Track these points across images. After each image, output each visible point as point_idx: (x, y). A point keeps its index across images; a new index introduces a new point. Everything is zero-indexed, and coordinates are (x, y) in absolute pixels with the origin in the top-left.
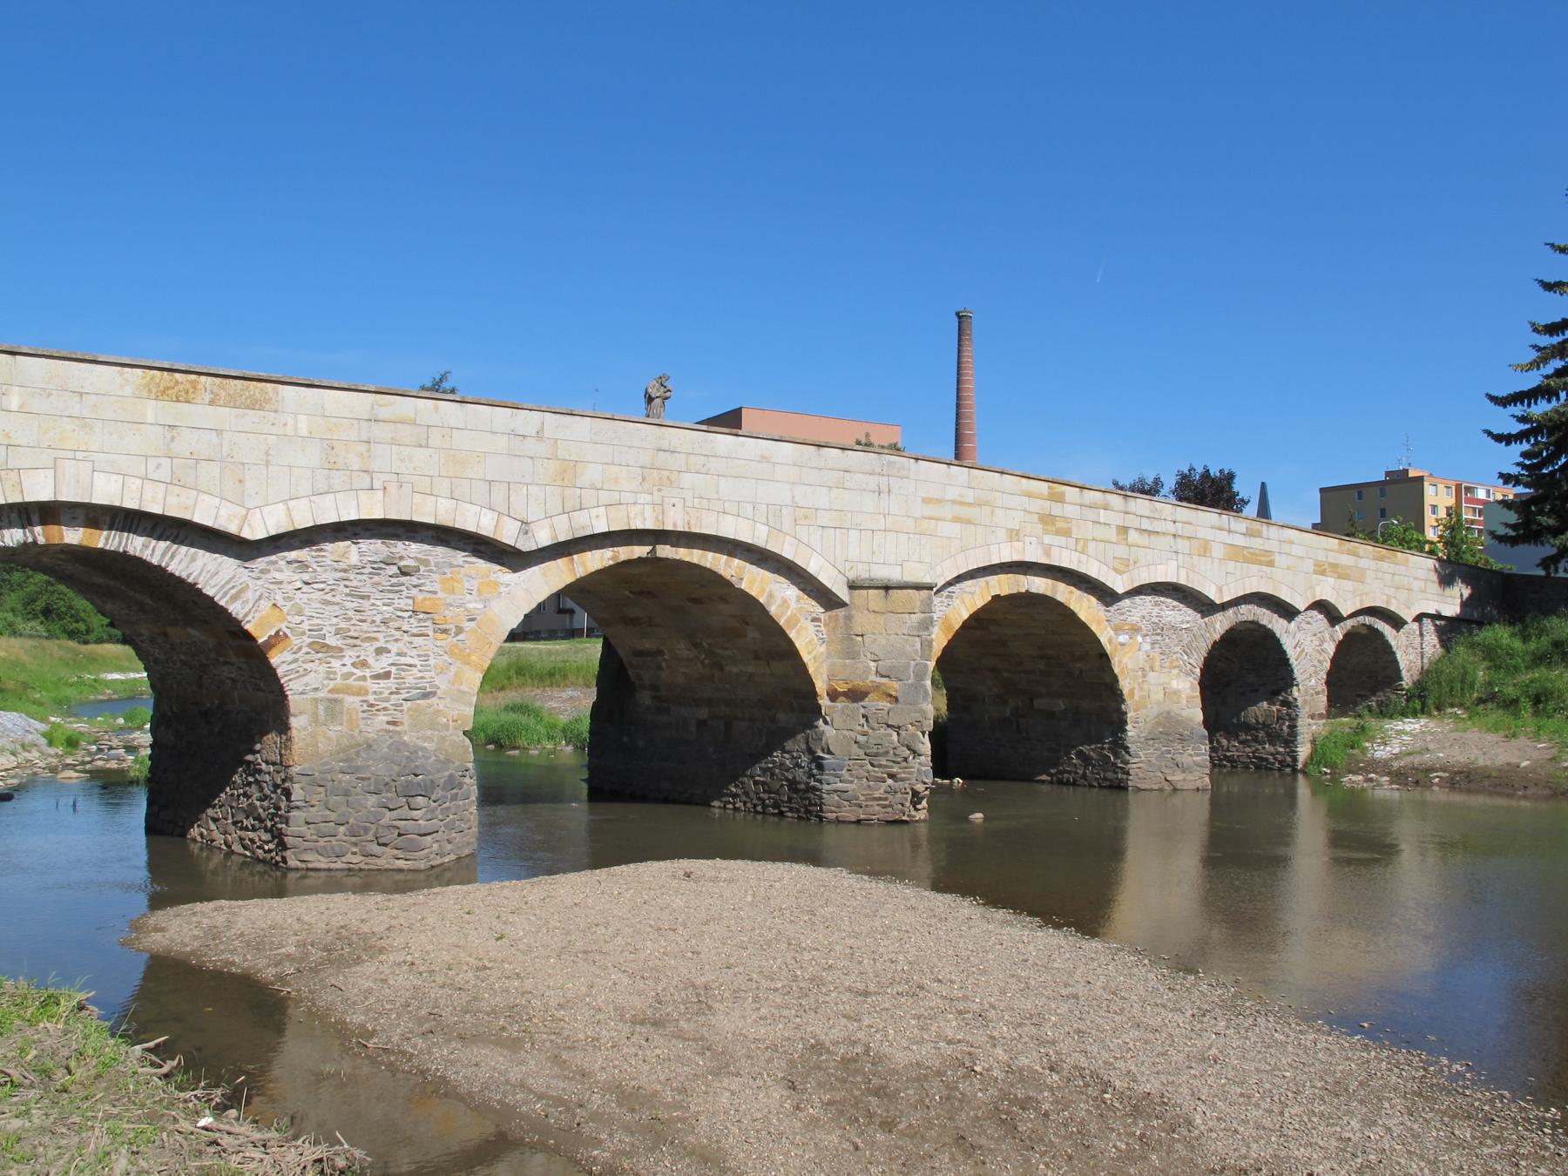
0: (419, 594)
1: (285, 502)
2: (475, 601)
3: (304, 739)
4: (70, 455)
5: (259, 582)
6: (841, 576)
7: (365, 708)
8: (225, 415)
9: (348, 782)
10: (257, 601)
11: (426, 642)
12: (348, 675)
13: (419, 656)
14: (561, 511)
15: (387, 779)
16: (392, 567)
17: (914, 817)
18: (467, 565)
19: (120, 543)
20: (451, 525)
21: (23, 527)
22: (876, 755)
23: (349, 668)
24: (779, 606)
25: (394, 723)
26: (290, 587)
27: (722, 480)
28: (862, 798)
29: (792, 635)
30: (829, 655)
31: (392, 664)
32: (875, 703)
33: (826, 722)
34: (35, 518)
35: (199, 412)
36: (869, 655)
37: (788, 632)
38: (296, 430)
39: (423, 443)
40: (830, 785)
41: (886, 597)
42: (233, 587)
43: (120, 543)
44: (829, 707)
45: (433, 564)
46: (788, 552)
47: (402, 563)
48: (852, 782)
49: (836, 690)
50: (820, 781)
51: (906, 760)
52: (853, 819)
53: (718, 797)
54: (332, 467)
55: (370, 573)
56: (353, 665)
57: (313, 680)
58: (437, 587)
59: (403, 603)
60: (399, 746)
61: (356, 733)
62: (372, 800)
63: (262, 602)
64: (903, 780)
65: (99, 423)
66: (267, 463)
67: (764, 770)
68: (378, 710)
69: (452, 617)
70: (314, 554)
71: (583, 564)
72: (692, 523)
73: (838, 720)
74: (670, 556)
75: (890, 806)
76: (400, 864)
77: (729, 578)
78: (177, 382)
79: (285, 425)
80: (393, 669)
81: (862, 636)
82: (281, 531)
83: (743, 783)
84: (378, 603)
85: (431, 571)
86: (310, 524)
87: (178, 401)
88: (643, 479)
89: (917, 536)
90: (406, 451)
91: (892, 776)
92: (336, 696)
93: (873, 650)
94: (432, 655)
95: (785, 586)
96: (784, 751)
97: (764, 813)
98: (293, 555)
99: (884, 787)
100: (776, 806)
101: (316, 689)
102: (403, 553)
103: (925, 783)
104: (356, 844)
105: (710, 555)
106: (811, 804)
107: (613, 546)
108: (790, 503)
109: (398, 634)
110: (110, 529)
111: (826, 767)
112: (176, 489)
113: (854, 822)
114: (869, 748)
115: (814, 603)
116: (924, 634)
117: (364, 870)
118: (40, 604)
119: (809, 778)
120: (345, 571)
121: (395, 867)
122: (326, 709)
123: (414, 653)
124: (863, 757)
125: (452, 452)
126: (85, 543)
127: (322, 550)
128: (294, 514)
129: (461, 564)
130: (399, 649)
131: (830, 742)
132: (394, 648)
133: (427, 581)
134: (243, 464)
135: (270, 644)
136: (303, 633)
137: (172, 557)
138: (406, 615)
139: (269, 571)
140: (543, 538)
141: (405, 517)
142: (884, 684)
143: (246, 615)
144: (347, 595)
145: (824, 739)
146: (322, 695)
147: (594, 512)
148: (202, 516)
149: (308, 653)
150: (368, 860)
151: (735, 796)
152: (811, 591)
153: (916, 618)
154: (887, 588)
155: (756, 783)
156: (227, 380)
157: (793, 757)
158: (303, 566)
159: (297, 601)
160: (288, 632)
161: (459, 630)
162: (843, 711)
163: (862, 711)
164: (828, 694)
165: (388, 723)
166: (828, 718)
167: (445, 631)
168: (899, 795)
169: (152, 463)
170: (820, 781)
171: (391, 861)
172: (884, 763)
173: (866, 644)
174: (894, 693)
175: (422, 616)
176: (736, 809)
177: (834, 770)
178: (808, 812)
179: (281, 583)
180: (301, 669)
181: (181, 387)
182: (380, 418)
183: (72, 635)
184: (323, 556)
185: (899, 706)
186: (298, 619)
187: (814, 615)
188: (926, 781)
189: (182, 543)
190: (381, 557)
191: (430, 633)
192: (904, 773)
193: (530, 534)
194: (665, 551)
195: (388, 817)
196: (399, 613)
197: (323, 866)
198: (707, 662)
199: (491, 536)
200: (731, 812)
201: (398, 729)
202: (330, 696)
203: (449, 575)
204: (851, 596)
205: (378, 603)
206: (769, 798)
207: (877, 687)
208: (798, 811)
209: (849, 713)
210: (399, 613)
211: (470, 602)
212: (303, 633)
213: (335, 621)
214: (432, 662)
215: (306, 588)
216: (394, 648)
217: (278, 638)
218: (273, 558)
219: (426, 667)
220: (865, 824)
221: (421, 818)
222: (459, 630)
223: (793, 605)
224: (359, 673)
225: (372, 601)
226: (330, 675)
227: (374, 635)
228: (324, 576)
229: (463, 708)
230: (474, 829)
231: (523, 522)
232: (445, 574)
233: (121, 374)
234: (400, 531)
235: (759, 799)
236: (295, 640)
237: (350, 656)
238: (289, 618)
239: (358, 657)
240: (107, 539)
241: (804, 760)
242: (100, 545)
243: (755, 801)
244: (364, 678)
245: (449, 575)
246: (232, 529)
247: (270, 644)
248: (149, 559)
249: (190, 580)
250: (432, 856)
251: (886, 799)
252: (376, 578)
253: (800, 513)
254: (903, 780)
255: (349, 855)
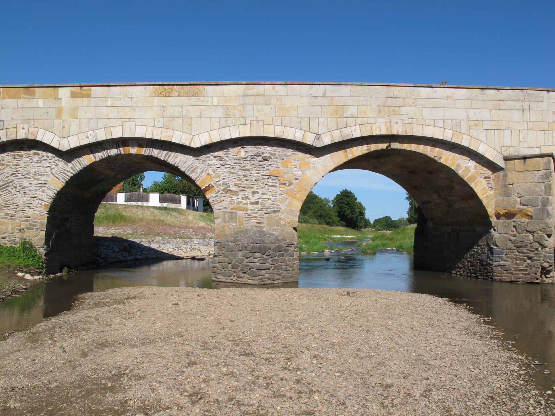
0: (271, 168)
1: (208, 132)
2: (298, 171)
3: (219, 228)
4: (128, 120)
5: (202, 165)
6: (499, 154)
7: (247, 216)
8: (184, 100)
9: (233, 246)
10: (201, 173)
11: (276, 189)
12: (239, 203)
13: (272, 195)
14: (336, 128)
15: (246, 245)
16: (259, 157)
17: (545, 281)
18: (294, 155)
19: (149, 153)
20: (281, 137)
21: (117, 148)
22: (521, 247)
23: (240, 200)
24: (463, 171)
25: (259, 223)
26: (215, 167)
27: (424, 109)
28: (513, 269)
29: (472, 185)
30: (495, 196)
31: (259, 198)
32: (520, 220)
33: (495, 230)
34: (120, 145)
35: (174, 100)
36: (516, 194)
37: (469, 184)
38: (212, 103)
39: (268, 103)
40: (497, 262)
41: (524, 163)
42: (192, 167)
43: (149, 153)
44: (496, 222)
45: (277, 155)
46: (465, 143)
47: (263, 156)
48: (508, 261)
49: (499, 213)
50: (491, 260)
51: (537, 249)
52: (508, 280)
53: (454, 268)
54: (227, 116)
55: (250, 160)
56: (242, 198)
57: (223, 204)
58: (280, 165)
59: (265, 172)
60: (261, 233)
61: (242, 227)
62: (240, 254)
63: (203, 173)
64: (536, 260)
65: (138, 108)
66: (201, 117)
67: (471, 255)
68: (252, 217)
69: (287, 178)
70: (225, 153)
71: (352, 153)
72: (408, 130)
73: (500, 228)
74: (399, 148)
75: (529, 274)
76: (250, 281)
77: (433, 157)
78: (165, 89)
79: (208, 101)
80: (260, 200)
81: (512, 184)
82: (207, 143)
83: (463, 262)
84: (253, 172)
85: (277, 158)
86: (219, 140)
87: (166, 96)
88: (380, 112)
89: (550, 132)
90: (260, 107)
91: (529, 258)
92: (233, 211)
93: (519, 192)
94: (278, 195)
95: (467, 161)
96: (479, 246)
97: (470, 276)
98: (216, 154)
99: (525, 264)
100: (475, 273)
101: (225, 208)
102: (264, 151)
103: (549, 263)
104: (234, 272)
105: (413, 145)
106: (488, 272)
107: (367, 144)
108: (465, 118)
109: (263, 186)
110: (146, 147)
111: (494, 253)
112: (165, 130)
113: (509, 282)
114: (516, 243)
115: (485, 169)
116: (546, 181)
117: (237, 283)
118: (318, 214)
119: (487, 259)
120: (239, 160)
121: (248, 283)
122: (229, 216)
123: (270, 193)
124: (514, 248)
125: (281, 106)
126: (137, 153)
127: (228, 151)
128: (212, 136)
129: (291, 155)
130: (263, 192)
131: (496, 240)
132: (261, 191)
133: (275, 163)
134: (191, 118)
135: (206, 189)
136: (220, 185)
137: (169, 157)
138: (266, 177)
139: (206, 161)
140: (327, 141)
141: (260, 134)
142: (525, 209)
143: (197, 178)
144: (239, 169)
145: (493, 239)
146: (228, 210)
147: (353, 128)
148: (175, 140)
149: (222, 193)
150: (239, 279)
151: (460, 268)
152: (484, 163)
153: (543, 172)
154: (525, 158)
155: (468, 262)
156: (184, 86)
157: (482, 249)
158: (220, 158)
159: (218, 172)
160: (214, 185)
161: (291, 184)
162: (503, 224)
163: (513, 224)
164: (495, 216)
165: (257, 223)
166: (495, 228)
167: (284, 184)
168: (534, 269)
169: (157, 120)
170: (491, 260)
171: (247, 280)
172: (525, 251)
173: (514, 189)
174: (530, 214)
175: (273, 178)
176: (461, 275)
177: (498, 254)
178: (487, 276)
179: (211, 165)
180: (219, 200)
181: (167, 91)
182: (249, 94)
183: (328, 224)
184: (229, 154)
185: (533, 220)
186: (218, 179)
187: (486, 175)
188: (549, 261)
189: (172, 151)
190: (254, 153)
191: (278, 185)
192: (536, 257)
193: (320, 139)
194: (396, 145)
195: (246, 261)
196: (263, 177)
197: (223, 280)
198: (446, 204)
199: (301, 141)
200: (458, 276)
201: (261, 225)
202: (231, 211)
203: (285, 160)
204: (506, 165)
205: (253, 172)
206: (473, 269)
207: (521, 211)
208: (483, 276)
209: (506, 225)
210: (263, 177)
211: (296, 171)
212: (220, 185)
213: (234, 180)
214: (278, 197)
215: (222, 167)
216: (261, 191)
217: (210, 187)
218: (208, 155)
219: (275, 200)
220: (515, 283)
221: (257, 262)
222: (291, 184)
223: (472, 170)
224: (244, 202)
225: (251, 172)
226: (232, 202)
227: (252, 186)
228: (229, 162)
229: (292, 217)
230: (296, 270)
231: (316, 134)
232: (283, 159)
233: (145, 89)
234: (262, 142)
235: (469, 269)
236: (216, 188)
237: (241, 195)
238: (214, 179)
239: (245, 195)
240: (145, 151)
241: (486, 250)
242: (143, 154)
243: (467, 271)
244: (247, 204)
245: (285, 160)
246: (187, 144)
247: (206, 189)
248: (160, 158)
249: (176, 165)
250: (264, 279)
251: (526, 270)
252: (253, 162)
253: (472, 123)
254: (536, 260)
255: (232, 277)
